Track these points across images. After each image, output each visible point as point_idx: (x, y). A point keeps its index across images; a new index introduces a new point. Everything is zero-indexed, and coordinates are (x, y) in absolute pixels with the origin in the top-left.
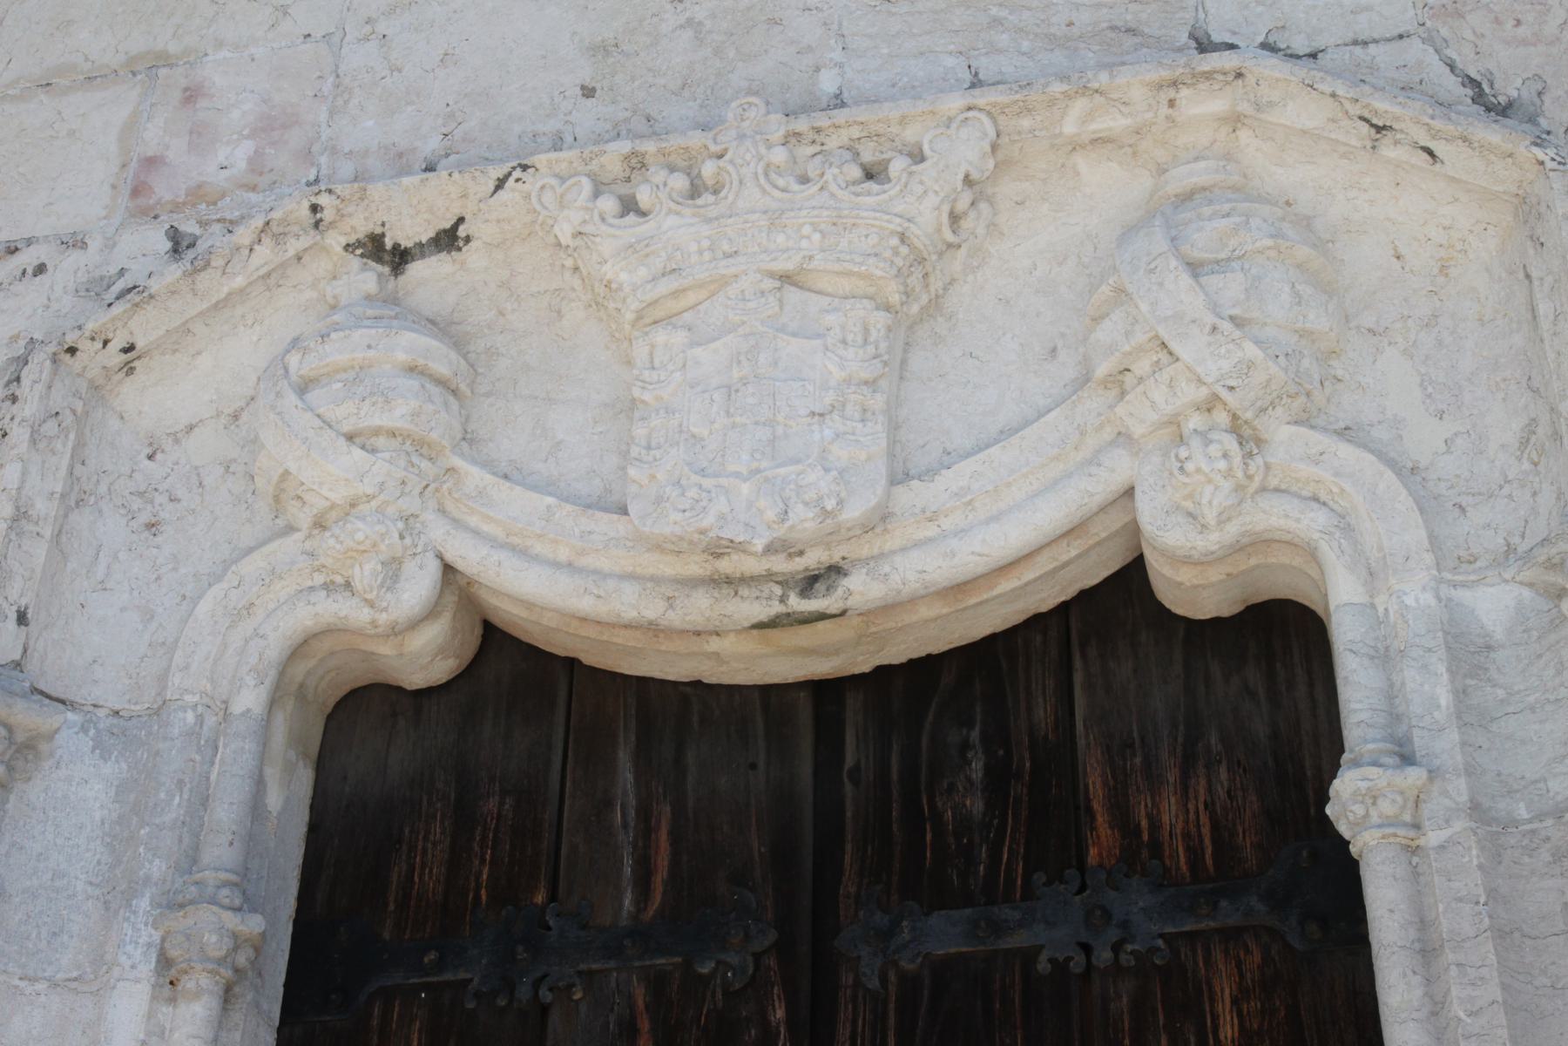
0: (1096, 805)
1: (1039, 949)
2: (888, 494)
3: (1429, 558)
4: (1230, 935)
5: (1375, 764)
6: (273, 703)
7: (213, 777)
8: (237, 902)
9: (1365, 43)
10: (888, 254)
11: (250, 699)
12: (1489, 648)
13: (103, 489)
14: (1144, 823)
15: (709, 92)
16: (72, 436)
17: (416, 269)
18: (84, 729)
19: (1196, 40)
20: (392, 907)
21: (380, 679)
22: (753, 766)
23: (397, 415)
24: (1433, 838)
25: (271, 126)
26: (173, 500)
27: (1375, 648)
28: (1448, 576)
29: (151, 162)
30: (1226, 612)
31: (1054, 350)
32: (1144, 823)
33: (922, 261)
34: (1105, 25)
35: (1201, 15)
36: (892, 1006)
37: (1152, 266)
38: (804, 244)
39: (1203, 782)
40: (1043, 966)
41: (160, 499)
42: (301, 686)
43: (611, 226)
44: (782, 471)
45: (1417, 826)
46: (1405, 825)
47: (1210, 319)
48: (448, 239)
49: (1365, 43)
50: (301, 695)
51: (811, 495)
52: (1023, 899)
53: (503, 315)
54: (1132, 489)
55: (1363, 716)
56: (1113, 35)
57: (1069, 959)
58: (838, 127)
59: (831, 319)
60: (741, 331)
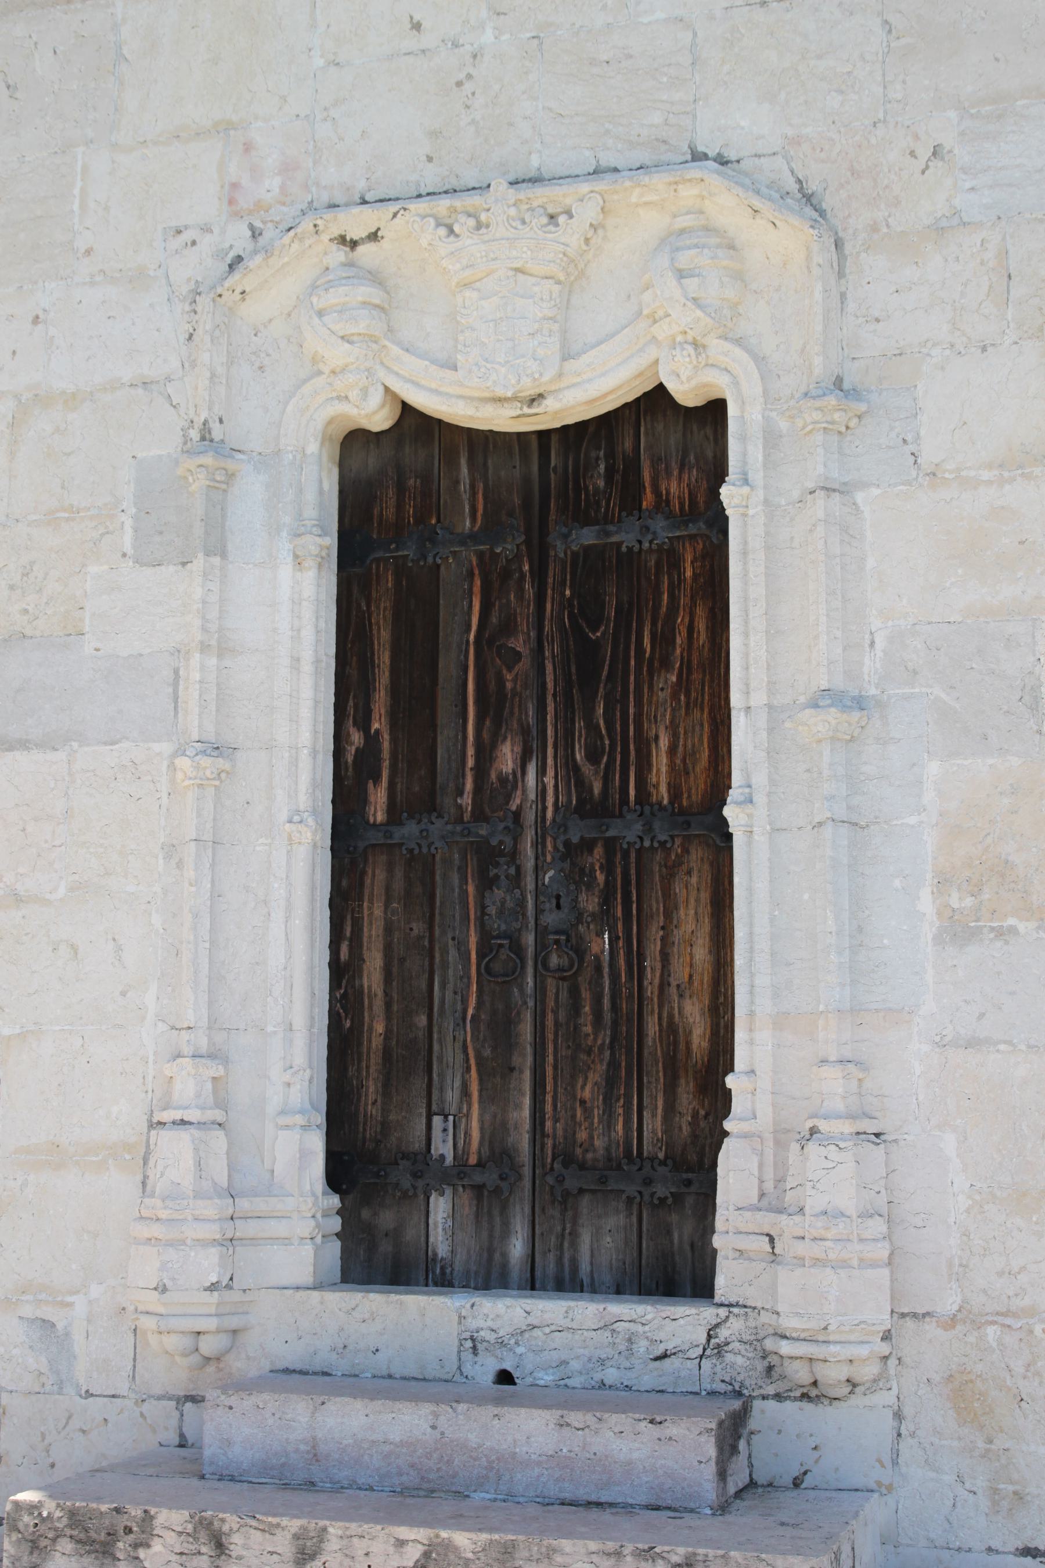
0: (647, 485)
1: (622, 543)
2: (561, 366)
3: (762, 400)
4: (692, 537)
5: (734, 485)
6: (322, 444)
7: (303, 480)
8: (320, 533)
9: (760, 156)
10: (558, 261)
11: (313, 448)
13: (239, 354)
14: (664, 492)
16: (226, 335)
17: (361, 249)
18: (249, 462)
19: (691, 149)
20: (375, 525)
21: (362, 427)
22: (515, 467)
23: (361, 327)
24: (751, 512)
25: (287, 168)
26: (268, 355)
27: (741, 435)
29: (235, 186)
30: (699, 404)
31: (629, 296)
32: (664, 492)
33: (573, 261)
34: (653, 137)
35: (694, 135)
36: (569, 564)
38: (524, 255)
39: (687, 475)
40: (624, 549)
41: (263, 355)
42: (331, 435)
43: (444, 242)
44: (518, 361)
45: (747, 507)
46: (743, 506)
47: (683, 300)
48: (374, 236)
49: (760, 156)
50: (331, 439)
51: (529, 372)
52: (618, 522)
54: (658, 360)
57: (633, 546)
58: (537, 197)
59: (536, 289)
60: (500, 295)
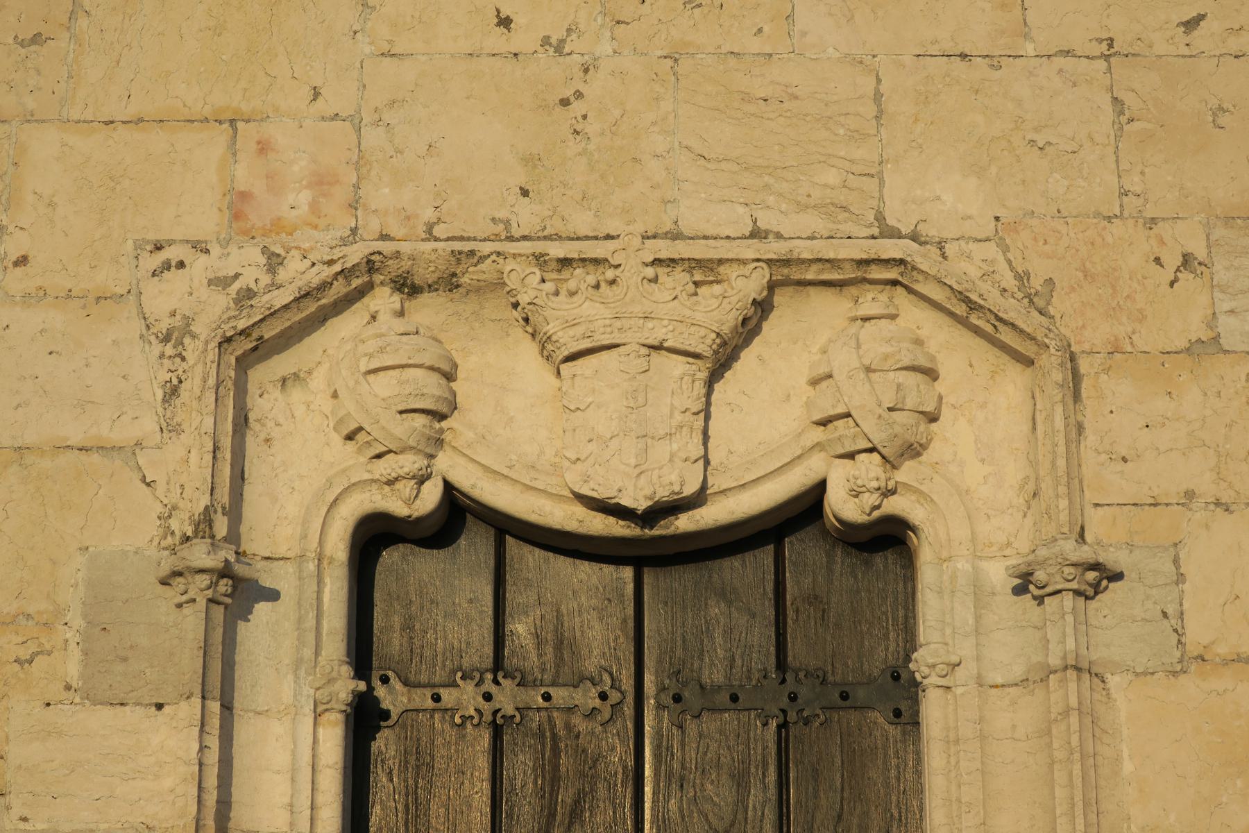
12: (994, 594)
15: (599, 206)
26: (278, 425)
28: (979, 554)
29: (244, 196)
31: (789, 396)
34: (829, 201)
35: (882, 205)
37: (851, 374)
53: (473, 329)
55: (933, 623)
56: (833, 209)
